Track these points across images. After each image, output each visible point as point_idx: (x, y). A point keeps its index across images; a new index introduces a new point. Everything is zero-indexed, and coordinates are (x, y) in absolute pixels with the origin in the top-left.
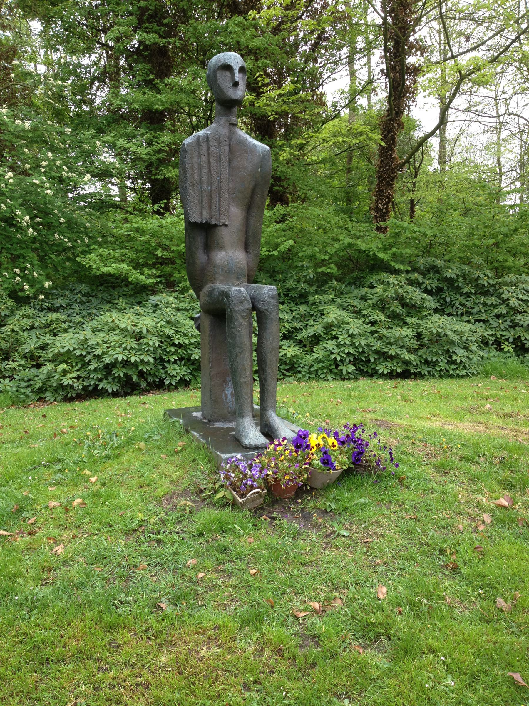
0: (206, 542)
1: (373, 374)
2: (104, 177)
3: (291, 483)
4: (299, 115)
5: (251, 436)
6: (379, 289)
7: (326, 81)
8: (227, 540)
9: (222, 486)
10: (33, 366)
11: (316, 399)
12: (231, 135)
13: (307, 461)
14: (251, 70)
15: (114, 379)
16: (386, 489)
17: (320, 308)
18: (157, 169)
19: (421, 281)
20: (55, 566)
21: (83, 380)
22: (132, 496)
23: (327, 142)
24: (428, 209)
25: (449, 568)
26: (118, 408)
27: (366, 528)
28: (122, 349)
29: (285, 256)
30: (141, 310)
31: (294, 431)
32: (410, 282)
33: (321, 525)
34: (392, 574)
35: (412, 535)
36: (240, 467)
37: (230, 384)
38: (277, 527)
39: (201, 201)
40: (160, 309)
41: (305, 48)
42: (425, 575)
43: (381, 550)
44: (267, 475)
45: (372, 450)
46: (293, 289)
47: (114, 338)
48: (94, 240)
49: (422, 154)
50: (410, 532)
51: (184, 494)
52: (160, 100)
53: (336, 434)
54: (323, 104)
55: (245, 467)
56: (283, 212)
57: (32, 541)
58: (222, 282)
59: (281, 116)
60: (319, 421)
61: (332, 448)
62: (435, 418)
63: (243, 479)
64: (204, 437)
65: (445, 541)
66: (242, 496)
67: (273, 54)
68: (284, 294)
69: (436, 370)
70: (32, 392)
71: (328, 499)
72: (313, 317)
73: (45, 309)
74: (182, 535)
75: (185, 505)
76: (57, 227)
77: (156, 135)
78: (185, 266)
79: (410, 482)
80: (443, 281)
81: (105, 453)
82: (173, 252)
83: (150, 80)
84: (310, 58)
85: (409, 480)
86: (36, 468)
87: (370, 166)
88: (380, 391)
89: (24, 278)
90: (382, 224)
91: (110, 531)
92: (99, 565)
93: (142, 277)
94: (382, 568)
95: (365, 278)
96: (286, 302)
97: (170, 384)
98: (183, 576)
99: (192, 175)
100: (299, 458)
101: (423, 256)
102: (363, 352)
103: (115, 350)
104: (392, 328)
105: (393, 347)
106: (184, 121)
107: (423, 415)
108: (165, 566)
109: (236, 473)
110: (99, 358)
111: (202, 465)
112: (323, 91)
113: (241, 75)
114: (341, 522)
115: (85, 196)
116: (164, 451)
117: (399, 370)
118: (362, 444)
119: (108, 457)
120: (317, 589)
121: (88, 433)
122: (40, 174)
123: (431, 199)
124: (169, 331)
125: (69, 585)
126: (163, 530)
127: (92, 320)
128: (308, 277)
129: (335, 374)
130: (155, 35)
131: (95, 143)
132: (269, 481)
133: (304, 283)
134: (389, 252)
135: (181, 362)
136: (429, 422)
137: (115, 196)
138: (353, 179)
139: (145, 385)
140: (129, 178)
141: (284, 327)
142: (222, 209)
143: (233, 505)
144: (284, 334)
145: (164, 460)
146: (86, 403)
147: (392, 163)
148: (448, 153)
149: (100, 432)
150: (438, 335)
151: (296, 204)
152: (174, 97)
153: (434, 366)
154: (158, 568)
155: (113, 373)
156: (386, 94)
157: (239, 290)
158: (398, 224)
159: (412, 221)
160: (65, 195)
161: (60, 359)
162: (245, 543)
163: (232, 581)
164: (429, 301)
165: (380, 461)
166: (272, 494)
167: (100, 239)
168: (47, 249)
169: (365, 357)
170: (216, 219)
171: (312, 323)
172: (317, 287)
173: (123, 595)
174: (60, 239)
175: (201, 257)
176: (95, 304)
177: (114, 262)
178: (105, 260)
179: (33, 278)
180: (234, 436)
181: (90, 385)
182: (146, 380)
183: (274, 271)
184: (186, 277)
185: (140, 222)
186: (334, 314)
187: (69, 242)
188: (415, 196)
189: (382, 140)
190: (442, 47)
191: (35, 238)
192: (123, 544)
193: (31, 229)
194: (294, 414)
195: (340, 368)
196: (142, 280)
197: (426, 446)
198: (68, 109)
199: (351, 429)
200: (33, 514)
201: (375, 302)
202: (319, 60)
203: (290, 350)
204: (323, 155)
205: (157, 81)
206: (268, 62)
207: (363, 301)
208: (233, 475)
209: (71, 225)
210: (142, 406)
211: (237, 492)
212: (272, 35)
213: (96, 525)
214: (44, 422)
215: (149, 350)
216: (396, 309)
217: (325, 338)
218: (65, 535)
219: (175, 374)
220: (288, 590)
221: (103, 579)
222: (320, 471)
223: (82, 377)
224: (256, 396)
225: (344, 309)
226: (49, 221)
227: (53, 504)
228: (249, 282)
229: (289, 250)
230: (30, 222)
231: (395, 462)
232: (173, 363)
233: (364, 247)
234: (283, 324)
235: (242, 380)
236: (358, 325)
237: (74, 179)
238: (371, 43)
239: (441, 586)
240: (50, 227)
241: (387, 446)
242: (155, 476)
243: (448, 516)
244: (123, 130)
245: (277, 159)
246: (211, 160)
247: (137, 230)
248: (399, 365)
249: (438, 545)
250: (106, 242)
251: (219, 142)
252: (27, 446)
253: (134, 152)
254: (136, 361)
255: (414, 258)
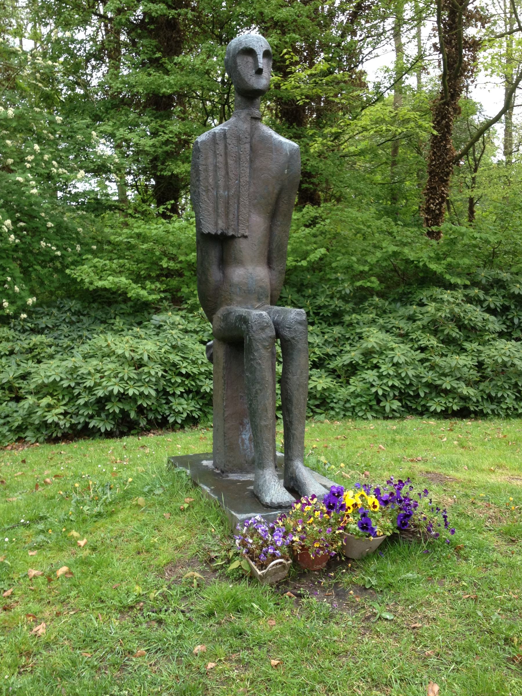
0: (217, 623)
1: (423, 412)
2: (100, 174)
3: (321, 552)
4: (334, 99)
5: (273, 492)
6: (431, 308)
7: (367, 57)
8: (243, 622)
9: (237, 554)
10: (12, 399)
11: (352, 445)
12: (254, 130)
13: (341, 525)
14: (277, 46)
15: (107, 416)
16: (439, 561)
17: (358, 331)
18: (163, 164)
19: (482, 298)
20: (35, 649)
21: (71, 417)
22: (128, 564)
23: (367, 130)
24: (491, 209)
25: (517, 662)
26: (112, 452)
27: (414, 611)
28: (118, 379)
29: (315, 266)
30: (141, 332)
31: (325, 486)
32: (469, 300)
33: (358, 605)
34: (446, 668)
35: (471, 620)
36: (260, 531)
37: (248, 427)
38: (304, 606)
39: (216, 209)
40: (164, 331)
41: (342, 18)
42: (486, 670)
43: (432, 638)
44: (293, 542)
45: (421, 513)
46: (325, 306)
47: (109, 366)
48: (87, 248)
49: (483, 143)
50: (468, 616)
51: (190, 564)
52: (168, 83)
53: (377, 491)
54: (363, 85)
55: (265, 531)
56: (313, 214)
57: (7, 618)
58: (239, 303)
59: (312, 100)
60: (356, 473)
61: (372, 509)
62: (500, 471)
63: (262, 546)
64: (216, 491)
65: (511, 628)
66: (262, 566)
67: (303, 27)
68: (314, 313)
69: (502, 408)
70: (10, 430)
71: (367, 573)
72: (350, 342)
73: (27, 330)
74: (188, 615)
75: (192, 577)
76: (44, 232)
77: (163, 123)
78: (195, 278)
79: (470, 552)
80: (510, 298)
81: (97, 509)
82: (181, 262)
83: (156, 58)
84: (348, 30)
85: (467, 550)
86: (13, 528)
87: (421, 158)
88: (432, 434)
90: (434, 228)
91: (102, 608)
92: (88, 650)
93: (144, 293)
94: (434, 660)
95: (413, 294)
96: (317, 322)
97: (175, 422)
98: (189, 666)
99: (206, 178)
100: (332, 521)
101: (485, 267)
102: (411, 385)
103: (110, 381)
104: (446, 356)
105: (448, 379)
106: (196, 106)
107: (485, 466)
108: (167, 653)
109: (255, 538)
110: (90, 390)
111: (213, 527)
112: (363, 69)
113: (266, 60)
114: (383, 602)
115: (77, 195)
116: (167, 508)
117: (455, 408)
118: (409, 505)
119: (99, 515)
120: (353, 686)
121: (77, 485)
122: (25, 170)
123: (495, 196)
124: (174, 358)
125: (51, 674)
126: (165, 607)
127: (83, 343)
128: (343, 293)
129: (376, 411)
130: (162, 6)
131: (90, 134)
132: (295, 548)
133: (338, 299)
134: (443, 262)
135: (188, 395)
136: (493, 476)
137: (112, 195)
138: (399, 174)
139: (145, 423)
140: (129, 173)
141: (314, 353)
142: (240, 218)
143: (251, 578)
144: (313, 361)
145: (167, 519)
146: (74, 445)
147: (447, 154)
148: (516, 142)
149: (91, 483)
150: (504, 364)
151: (329, 205)
152: (185, 78)
153: (499, 403)
154: (159, 655)
155: (107, 408)
156: (439, 72)
157: (260, 314)
158: (454, 229)
159: (471, 225)
160: (53, 196)
161: (44, 391)
162: (265, 627)
163: (249, 674)
164: (493, 323)
165: (431, 526)
166: (298, 565)
167: (94, 247)
168: (32, 259)
169: (413, 391)
170: (234, 229)
171: (348, 348)
172: (355, 304)
173: (116, 688)
175: (215, 274)
176: (87, 325)
177: (110, 275)
178: (100, 272)
179: (14, 293)
180: (252, 492)
181: (79, 423)
182: (146, 418)
183: (302, 285)
184: (196, 292)
185: (143, 226)
186: (375, 337)
187: (57, 250)
188: (476, 193)
189: (434, 128)
190: (508, 15)
191: (17, 246)
192: (117, 624)
193: (12, 236)
194: (325, 464)
195: (382, 404)
196: (143, 296)
197: (488, 506)
198: (58, 92)
199: (395, 485)
200: (9, 585)
201: (425, 324)
202: (359, 33)
203: (321, 382)
204: (362, 145)
205: (165, 60)
206: (297, 36)
207: (411, 322)
208: (251, 541)
209: (61, 230)
210: (141, 449)
211: (256, 562)
212: (302, 5)
213: (84, 600)
214: (24, 469)
215: (150, 381)
216: (451, 332)
217: (363, 367)
218: (48, 612)
219: (181, 410)
220: (317, 687)
221: (92, 668)
222: (357, 537)
223: (69, 413)
224: (280, 440)
225: (387, 331)
226: (34, 225)
227: (33, 572)
228: (272, 303)
229: (321, 259)
230: (11, 228)
231: (450, 526)
232: (179, 396)
233: (412, 256)
234: (313, 350)
235: (263, 423)
236: (405, 352)
237: (64, 176)
238: (421, 12)
239: (506, 684)
240: (36, 232)
241: (440, 507)
242: (156, 540)
243: (516, 596)
244: (123, 118)
245: (307, 151)
247: (139, 236)
248: (456, 401)
249: (502, 633)
250: (101, 250)
251: (239, 139)
252: (3, 500)
253: (137, 144)
254: (134, 394)
255: (473, 270)
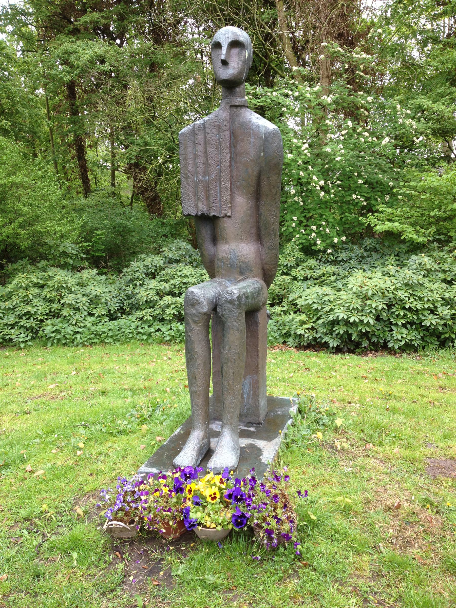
39: (196, 194)
70: (280, 335)
89: (318, 233)
135: (412, 326)
142: (222, 200)
174: (357, 198)
215: (371, 312)
246: (208, 148)
254: (354, 321)
